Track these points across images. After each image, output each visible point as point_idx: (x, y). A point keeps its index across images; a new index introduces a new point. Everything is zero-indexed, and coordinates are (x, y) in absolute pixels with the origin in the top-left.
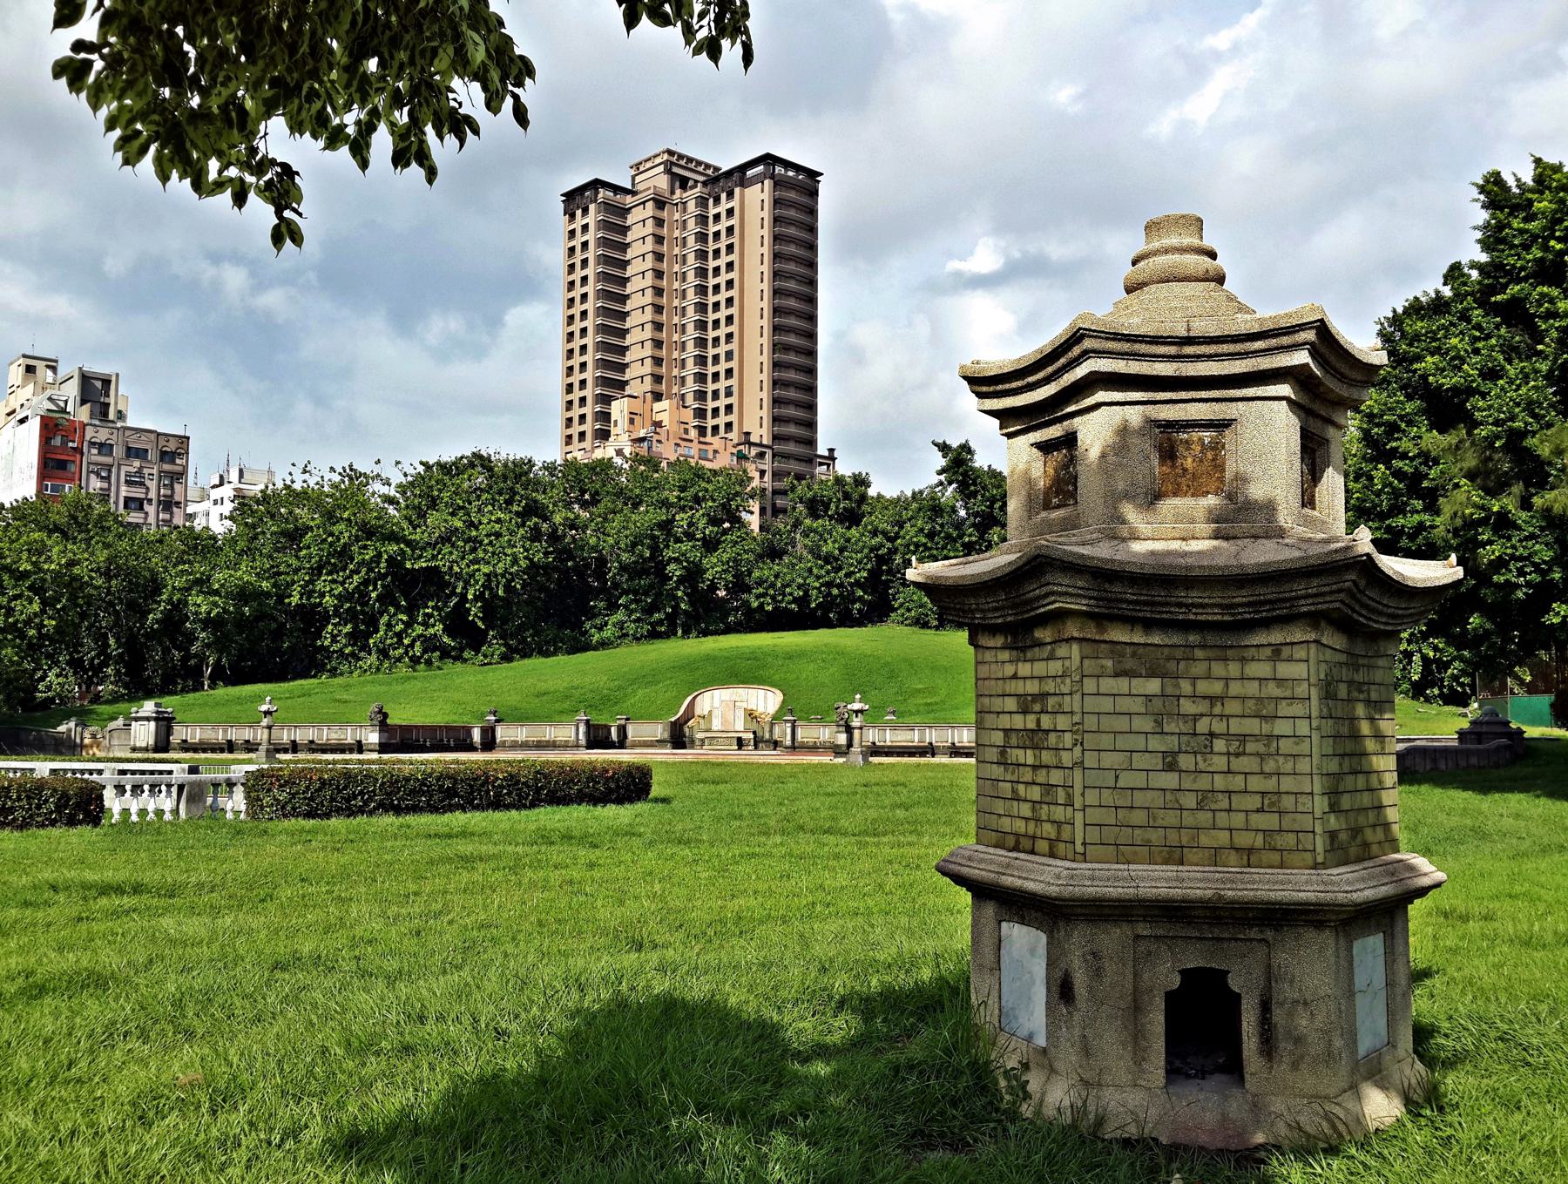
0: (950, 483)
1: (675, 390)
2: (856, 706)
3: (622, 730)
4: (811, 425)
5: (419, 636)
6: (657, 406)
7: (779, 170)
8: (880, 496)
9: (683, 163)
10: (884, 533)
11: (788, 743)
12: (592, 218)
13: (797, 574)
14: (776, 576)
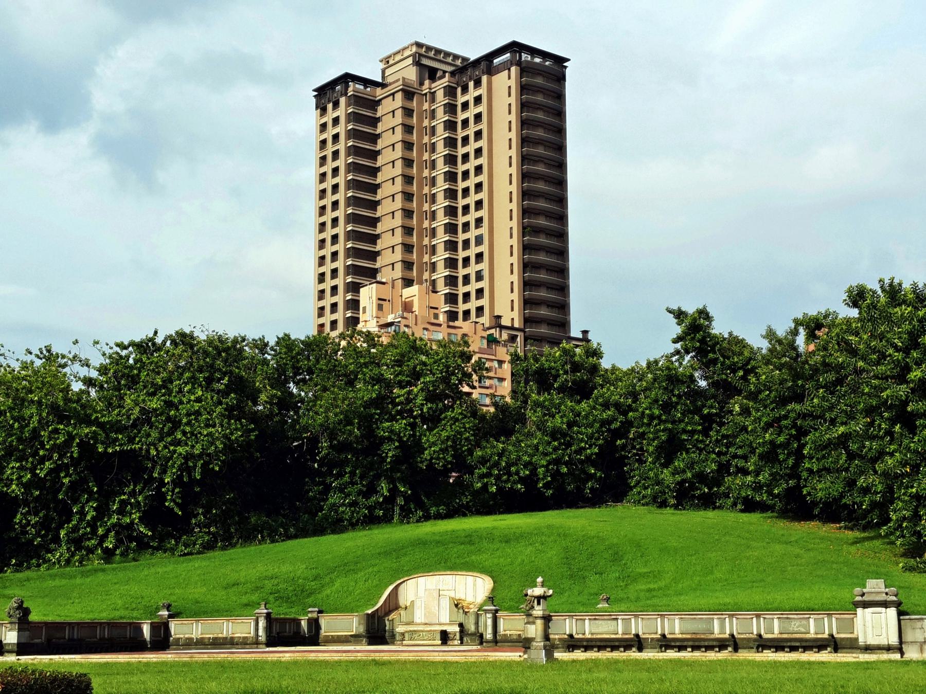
0: (687, 352)
1: (426, 275)
2: (538, 591)
3: (315, 624)
4: (564, 307)
5: (114, 525)
6: (408, 292)
7: (525, 57)
8: (614, 369)
9: (432, 54)
10: (617, 405)
11: (489, 636)
12: (341, 112)
13: (529, 450)
14: (500, 455)
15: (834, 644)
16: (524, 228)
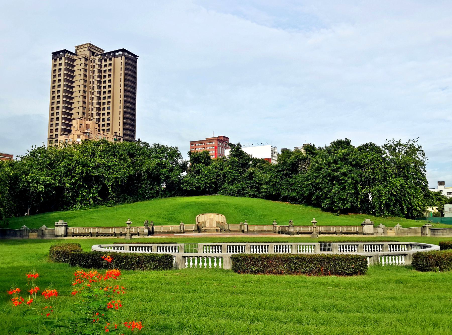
4: (134, 131)
5: (91, 197)
9: (94, 48)
15: (357, 233)
16: (124, 106)
